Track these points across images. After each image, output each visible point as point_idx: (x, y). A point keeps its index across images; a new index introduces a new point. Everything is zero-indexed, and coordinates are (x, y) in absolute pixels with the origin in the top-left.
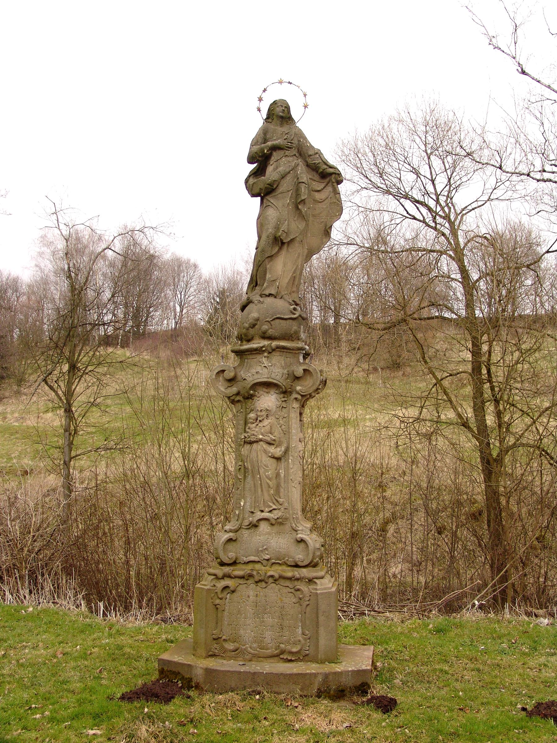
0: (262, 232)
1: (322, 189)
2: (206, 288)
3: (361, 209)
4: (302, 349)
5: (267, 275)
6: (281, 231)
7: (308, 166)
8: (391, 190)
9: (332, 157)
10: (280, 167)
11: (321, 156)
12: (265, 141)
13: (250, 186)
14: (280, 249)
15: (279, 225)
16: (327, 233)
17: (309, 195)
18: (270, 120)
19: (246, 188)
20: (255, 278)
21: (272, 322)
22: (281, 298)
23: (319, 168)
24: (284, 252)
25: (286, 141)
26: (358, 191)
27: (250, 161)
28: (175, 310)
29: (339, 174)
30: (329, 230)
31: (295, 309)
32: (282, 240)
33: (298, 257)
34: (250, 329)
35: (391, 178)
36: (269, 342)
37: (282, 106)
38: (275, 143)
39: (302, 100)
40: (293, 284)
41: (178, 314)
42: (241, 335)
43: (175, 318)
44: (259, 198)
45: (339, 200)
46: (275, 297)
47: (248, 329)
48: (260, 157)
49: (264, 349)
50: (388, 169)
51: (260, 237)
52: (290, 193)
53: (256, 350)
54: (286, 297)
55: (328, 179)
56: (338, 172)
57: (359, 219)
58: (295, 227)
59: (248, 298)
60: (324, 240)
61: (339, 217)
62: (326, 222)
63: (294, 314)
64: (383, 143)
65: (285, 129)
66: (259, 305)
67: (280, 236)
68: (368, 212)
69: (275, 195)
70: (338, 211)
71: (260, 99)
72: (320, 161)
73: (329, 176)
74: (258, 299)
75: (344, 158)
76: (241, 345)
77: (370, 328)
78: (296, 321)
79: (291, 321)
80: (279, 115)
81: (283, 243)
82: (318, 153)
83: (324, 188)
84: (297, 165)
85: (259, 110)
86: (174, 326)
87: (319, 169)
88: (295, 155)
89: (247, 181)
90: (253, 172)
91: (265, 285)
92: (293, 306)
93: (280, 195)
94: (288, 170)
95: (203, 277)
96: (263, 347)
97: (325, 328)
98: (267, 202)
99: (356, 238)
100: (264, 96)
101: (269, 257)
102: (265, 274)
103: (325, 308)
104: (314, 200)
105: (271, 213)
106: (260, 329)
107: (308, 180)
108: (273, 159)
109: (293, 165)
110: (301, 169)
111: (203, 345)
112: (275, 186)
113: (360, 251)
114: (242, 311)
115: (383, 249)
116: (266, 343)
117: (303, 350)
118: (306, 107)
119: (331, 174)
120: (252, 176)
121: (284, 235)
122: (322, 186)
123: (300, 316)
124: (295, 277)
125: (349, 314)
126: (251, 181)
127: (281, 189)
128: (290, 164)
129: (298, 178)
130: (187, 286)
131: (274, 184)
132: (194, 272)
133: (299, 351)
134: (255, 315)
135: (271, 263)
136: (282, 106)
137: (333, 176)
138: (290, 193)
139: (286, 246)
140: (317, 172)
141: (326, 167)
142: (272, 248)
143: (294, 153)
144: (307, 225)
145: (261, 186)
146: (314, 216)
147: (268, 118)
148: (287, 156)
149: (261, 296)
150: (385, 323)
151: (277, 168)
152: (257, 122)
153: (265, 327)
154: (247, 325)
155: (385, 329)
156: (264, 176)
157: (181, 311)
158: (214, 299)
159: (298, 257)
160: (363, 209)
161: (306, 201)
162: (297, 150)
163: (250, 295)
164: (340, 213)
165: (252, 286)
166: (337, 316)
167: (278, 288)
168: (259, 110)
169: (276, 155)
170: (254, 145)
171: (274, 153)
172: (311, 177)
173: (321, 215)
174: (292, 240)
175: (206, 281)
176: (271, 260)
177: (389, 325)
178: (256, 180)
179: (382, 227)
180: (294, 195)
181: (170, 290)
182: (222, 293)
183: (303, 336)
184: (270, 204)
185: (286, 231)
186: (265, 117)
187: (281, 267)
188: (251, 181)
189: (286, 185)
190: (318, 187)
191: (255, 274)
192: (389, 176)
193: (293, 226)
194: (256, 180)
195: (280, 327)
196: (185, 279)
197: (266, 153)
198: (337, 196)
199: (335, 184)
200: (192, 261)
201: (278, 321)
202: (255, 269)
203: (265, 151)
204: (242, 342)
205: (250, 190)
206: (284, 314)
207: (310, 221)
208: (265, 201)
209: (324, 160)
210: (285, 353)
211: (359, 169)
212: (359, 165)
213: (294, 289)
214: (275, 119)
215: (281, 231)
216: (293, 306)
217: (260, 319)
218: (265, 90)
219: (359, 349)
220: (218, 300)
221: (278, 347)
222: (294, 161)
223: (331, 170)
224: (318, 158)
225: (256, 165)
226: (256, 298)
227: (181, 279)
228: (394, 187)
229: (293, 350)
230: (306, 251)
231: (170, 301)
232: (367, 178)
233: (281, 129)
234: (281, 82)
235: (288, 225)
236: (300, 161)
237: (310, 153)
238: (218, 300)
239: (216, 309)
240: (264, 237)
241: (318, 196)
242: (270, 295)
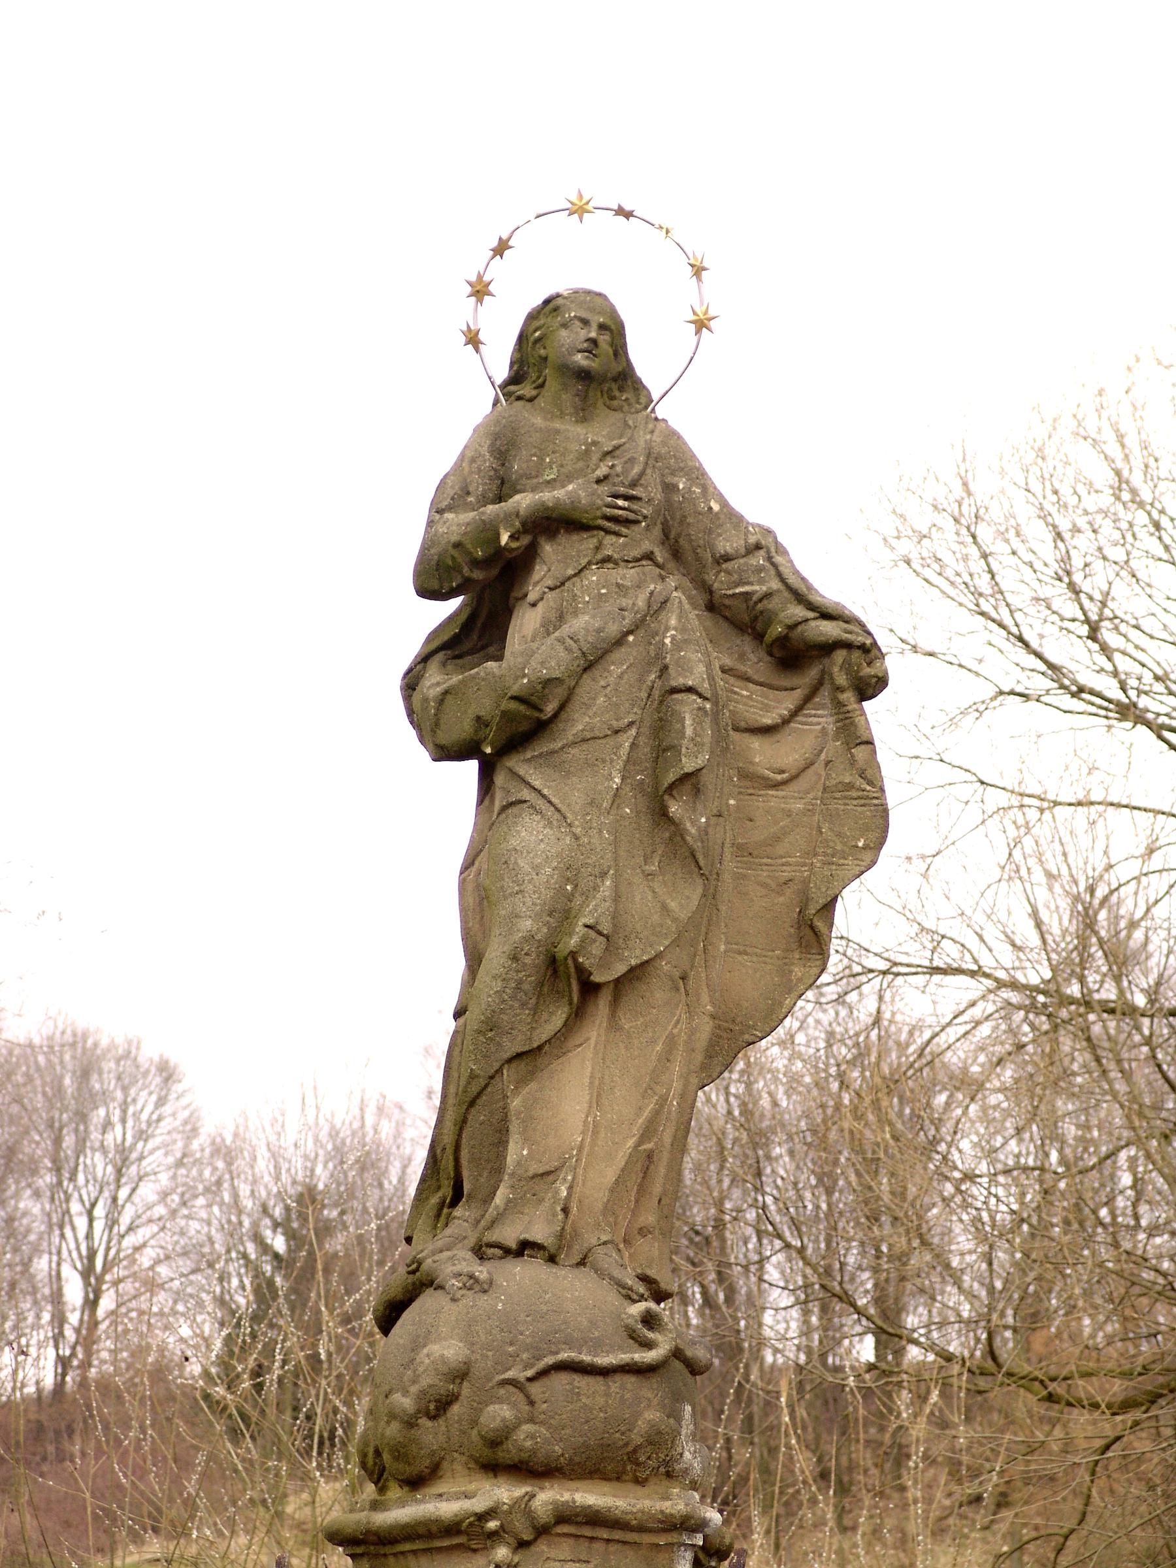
0: (486, 934)
1: (786, 722)
2: (219, 1183)
3: (997, 799)
4: (687, 1524)
5: (511, 1146)
6: (580, 929)
7: (712, 606)
8: (1143, 702)
9: (838, 564)
10: (576, 613)
11: (778, 559)
12: (503, 489)
13: (425, 709)
14: (578, 1014)
15: (570, 898)
16: (811, 933)
17: (721, 746)
18: (526, 390)
19: (410, 713)
20: (448, 1163)
21: (535, 1389)
22: (582, 1263)
23: (768, 618)
24: (594, 1031)
25: (604, 489)
26: (979, 709)
27: (431, 584)
28: (57, 1298)
29: (870, 650)
30: (819, 924)
31: (650, 1320)
32: (581, 971)
33: (667, 1057)
34: (424, 1422)
35: (1143, 641)
36: (520, 1491)
37: (585, 322)
38: (548, 496)
39: (685, 296)
40: (642, 1190)
41: (74, 1318)
42: (378, 1453)
43: (58, 1338)
44: (471, 767)
45: (871, 776)
46: (552, 1259)
47: (410, 1423)
48: (475, 563)
49: (492, 1525)
50: (1126, 600)
51: (474, 958)
52: (626, 741)
53: (452, 1528)
54: (606, 1258)
55: (813, 673)
56: (861, 639)
57: (985, 852)
58: (649, 905)
59: (415, 1267)
60: (798, 971)
61: (867, 856)
62: (806, 882)
63: (648, 1345)
64: (1104, 477)
65: (600, 431)
66: (469, 1299)
67: (573, 954)
68: (1033, 814)
69: (553, 752)
70: (864, 830)
71: (480, 291)
72: (775, 585)
73: (816, 658)
74: (463, 1267)
75: (906, 547)
76: (375, 1506)
77: (1051, 1398)
78: (654, 1380)
79: (631, 1380)
80: (572, 364)
81: (589, 989)
82: (763, 546)
83: (795, 713)
84: (657, 607)
85: (473, 340)
86: (49, 1382)
87: (768, 623)
88: (649, 556)
89: (411, 683)
90: (445, 637)
91: (499, 1199)
92: (642, 1306)
93: (574, 751)
94: (613, 629)
95: (207, 1129)
96: (483, 1517)
97: (822, 1390)
98: (513, 786)
99: (972, 942)
100: (499, 272)
101: (519, 1056)
102: (502, 1142)
103: (826, 1295)
104: (744, 775)
105: (533, 839)
106: (474, 1422)
107: (711, 678)
108: (541, 576)
109: (641, 603)
110: (682, 623)
111: (191, 1487)
112: (550, 708)
113: (991, 1008)
114: (386, 1331)
115: (1109, 993)
116: (503, 1492)
117: (694, 1530)
118: (701, 325)
119: (828, 648)
120: (440, 656)
121: (598, 947)
122: (786, 704)
123: (677, 1353)
124: (650, 1156)
125: (942, 1325)
126: (435, 681)
127: (579, 722)
128: (625, 602)
129: (665, 668)
130: (119, 1173)
131: (544, 698)
132: (161, 1102)
133: (673, 1538)
134: (449, 1350)
135: (533, 1085)
136: (585, 322)
137: (840, 655)
138: (626, 741)
139: (603, 1003)
140: (759, 637)
141: (799, 612)
142: (535, 1011)
143: (646, 546)
144: (710, 897)
145: (485, 709)
146: (742, 850)
147: (515, 379)
148: (607, 560)
149: (479, 1252)
150: (1126, 1375)
151: (561, 618)
152: (459, 402)
153: (499, 1413)
154: (405, 1403)
155: (1126, 1405)
156: (499, 658)
157: (91, 1304)
158: (258, 1239)
159: (667, 1057)
160: (1003, 799)
161: (707, 778)
162: (657, 531)
163: (424, 1246)
164: (873, 836)
165: (434, 1200)
166: (890, 1336)
167: (565, 1210)
168: (473, 340)
169: (555, 558)
170: (449, 508)
171: (548, 548)
172: (728, 662)
173: (780, 849)
174: (637, 973)
175: (220, 1150)
176: (532, 1074)
177: (1148, 1384)
178: (456, 679)
179: (1101, 892)
180: (645, 750)
181: (37, 1194)
182: (305, 1211)
183: (690, 1456)
184: (526, 794)
185: (605, 928)
186: (502, 373)
187: (580, 1108)
188: (435, 681)
189: (604, 702)
190: (767, 708)
191: (448, 1139)
192: (1134, 634)
193: (644, 900)
194: (456, 679)
195: (571, 1412)
196: (113, 1137)
197: (506, 548)
198: (860, 753)
199: (848, 697)
200: (148, 1054)
201: (561, 1380)
202: (450, 1116)
203: (504, 538)
204: (382, 1490)
205: (427, 726)
206: (597, 1346)
207: (727, 877)
208: (500, 779)
209: (792, 580)
210: (598, 1546)
211: (989, 606)
212: (983, 583)
213: (649, 1218)
214: (552, 385)
215: (580, 929)
216: (642, 1306)
217: (475, 1372)
218: (501, 248)
219: (1003, 1501)
220: (279, 1243)
221: (565, 1517)
222: (640, 586)
223: (829, 630)
224: (760, 569)
225: (455, 603)
226: (454, 1262)
227: (95, 1136)
228: (1159, 687)
229: (641, 1529)
230: (705, 1028)
231: (36, 1250)
232: (1026, 645)
233: (580, 430)
234: (579, 210)
235: (617, 897)
236: (674, 587)
237: (724, 545)
238: (279, 1243)
239: (264, 1292)
240: (496, 956)
241: (763, 754)
242: (525, 1248)
